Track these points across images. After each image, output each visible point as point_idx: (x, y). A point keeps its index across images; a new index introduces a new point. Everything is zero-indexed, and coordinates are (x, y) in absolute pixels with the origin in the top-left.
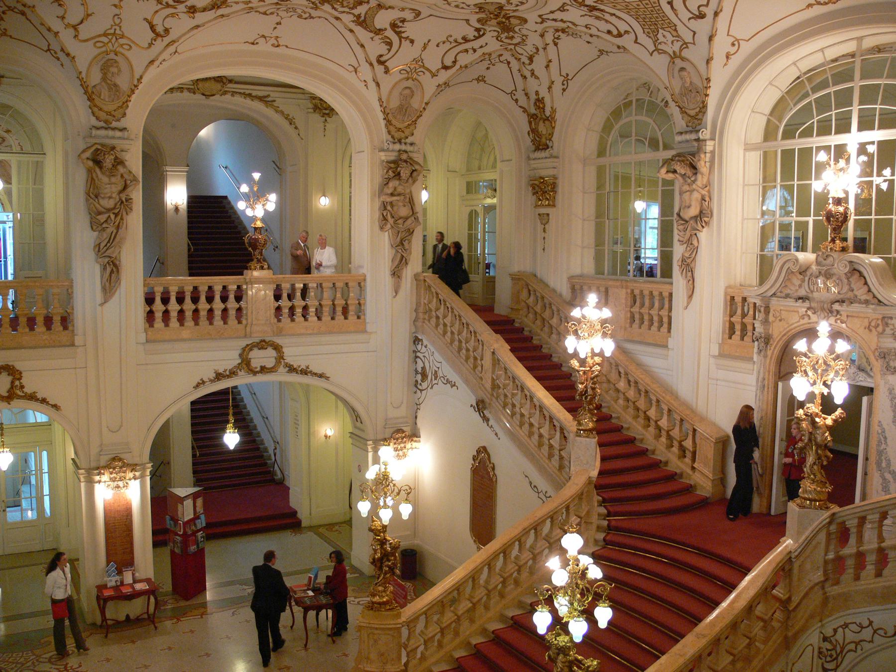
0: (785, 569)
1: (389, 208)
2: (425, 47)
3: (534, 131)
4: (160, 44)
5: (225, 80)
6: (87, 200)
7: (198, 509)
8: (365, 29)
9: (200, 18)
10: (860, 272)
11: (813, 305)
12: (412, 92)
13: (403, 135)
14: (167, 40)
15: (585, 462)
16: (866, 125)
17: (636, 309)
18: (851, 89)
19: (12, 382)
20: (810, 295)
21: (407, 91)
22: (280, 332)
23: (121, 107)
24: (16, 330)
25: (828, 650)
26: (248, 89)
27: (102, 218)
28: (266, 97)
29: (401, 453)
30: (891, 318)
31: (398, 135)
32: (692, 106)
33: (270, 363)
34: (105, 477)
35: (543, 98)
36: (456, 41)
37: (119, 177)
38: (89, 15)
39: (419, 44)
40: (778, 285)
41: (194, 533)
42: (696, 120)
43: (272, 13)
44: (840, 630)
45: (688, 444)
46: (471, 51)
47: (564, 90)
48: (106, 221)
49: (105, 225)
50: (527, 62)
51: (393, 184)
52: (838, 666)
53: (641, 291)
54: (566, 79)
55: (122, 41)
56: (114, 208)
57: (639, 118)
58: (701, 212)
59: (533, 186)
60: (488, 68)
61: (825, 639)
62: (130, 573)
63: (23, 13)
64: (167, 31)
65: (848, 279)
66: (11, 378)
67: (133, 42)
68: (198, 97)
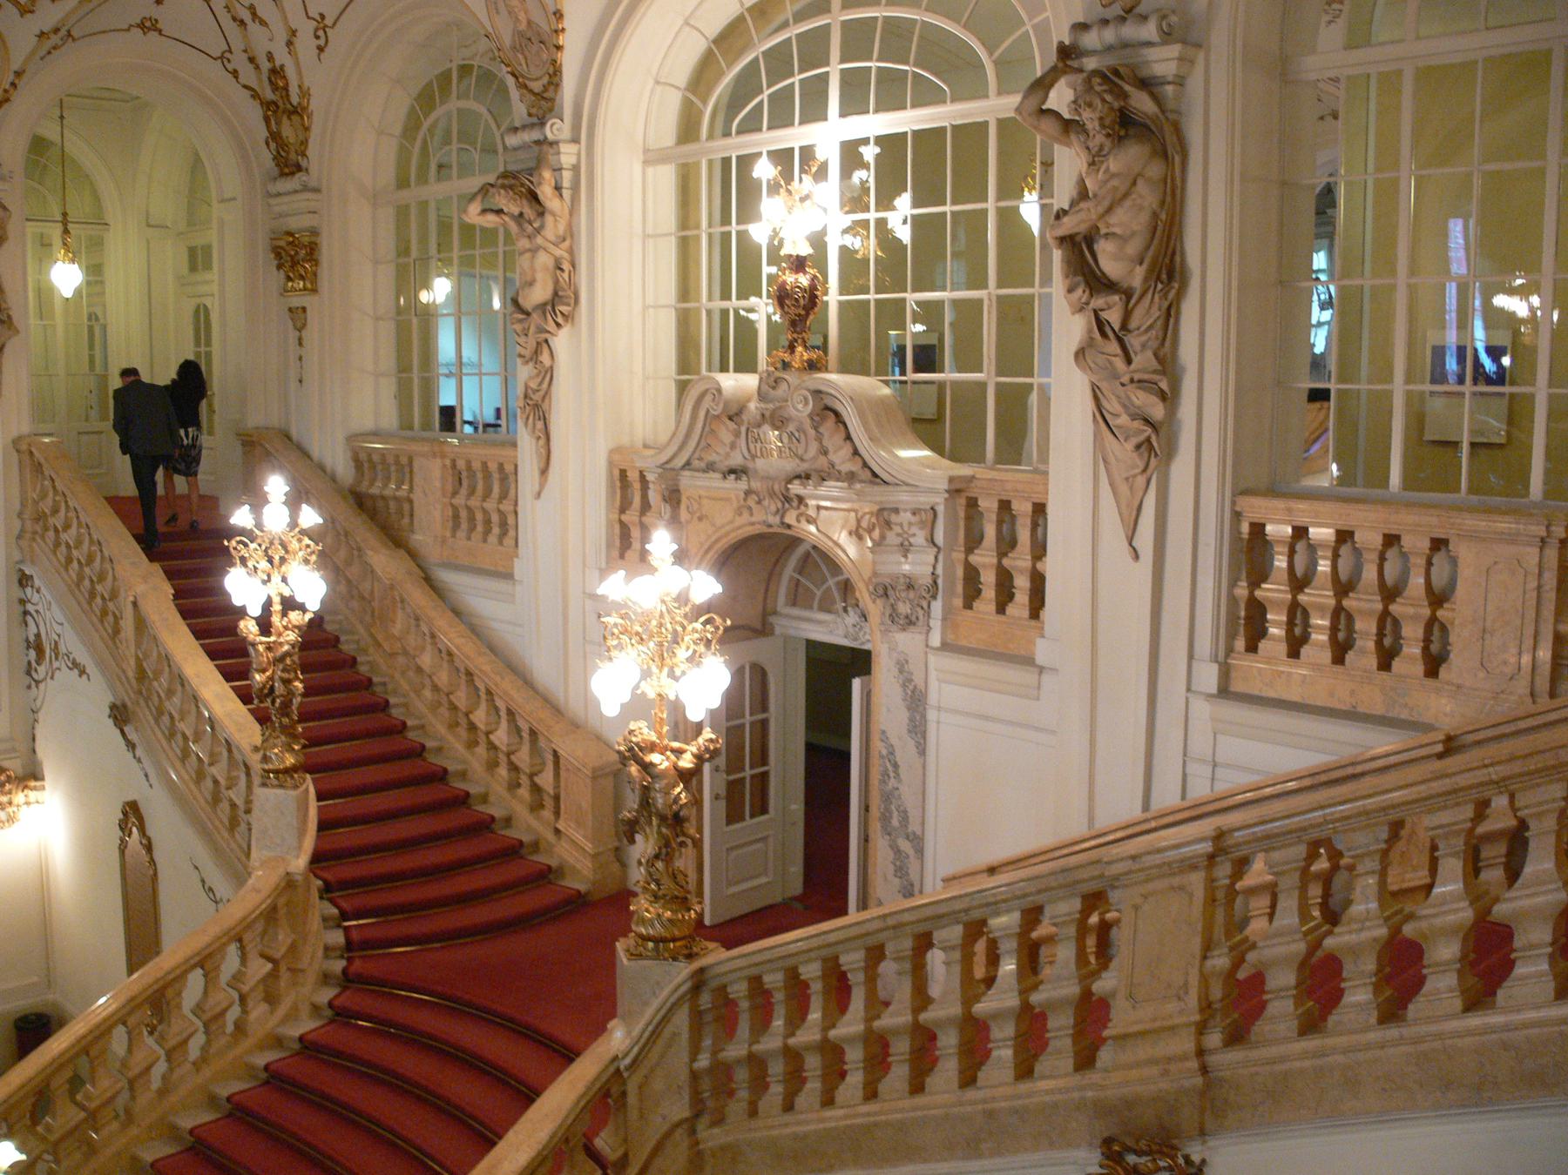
0: (606, 1100)
10: (837, 414)
11: (755, 485)
16: (853, 104)
17: (459, 500)
18: (826, 29)
20: (750, 465)
30: (896, 511)
32: (539, 73)
35: (282, 66)
40: (692, 444)
42: (544, 102)
45: (546, 780)
47: (321, 49)
53: (469, 463)
54: (322, 27)
57: (462, 104)
58: (556, 294)
59: (277, 252)
65: (816, 428)
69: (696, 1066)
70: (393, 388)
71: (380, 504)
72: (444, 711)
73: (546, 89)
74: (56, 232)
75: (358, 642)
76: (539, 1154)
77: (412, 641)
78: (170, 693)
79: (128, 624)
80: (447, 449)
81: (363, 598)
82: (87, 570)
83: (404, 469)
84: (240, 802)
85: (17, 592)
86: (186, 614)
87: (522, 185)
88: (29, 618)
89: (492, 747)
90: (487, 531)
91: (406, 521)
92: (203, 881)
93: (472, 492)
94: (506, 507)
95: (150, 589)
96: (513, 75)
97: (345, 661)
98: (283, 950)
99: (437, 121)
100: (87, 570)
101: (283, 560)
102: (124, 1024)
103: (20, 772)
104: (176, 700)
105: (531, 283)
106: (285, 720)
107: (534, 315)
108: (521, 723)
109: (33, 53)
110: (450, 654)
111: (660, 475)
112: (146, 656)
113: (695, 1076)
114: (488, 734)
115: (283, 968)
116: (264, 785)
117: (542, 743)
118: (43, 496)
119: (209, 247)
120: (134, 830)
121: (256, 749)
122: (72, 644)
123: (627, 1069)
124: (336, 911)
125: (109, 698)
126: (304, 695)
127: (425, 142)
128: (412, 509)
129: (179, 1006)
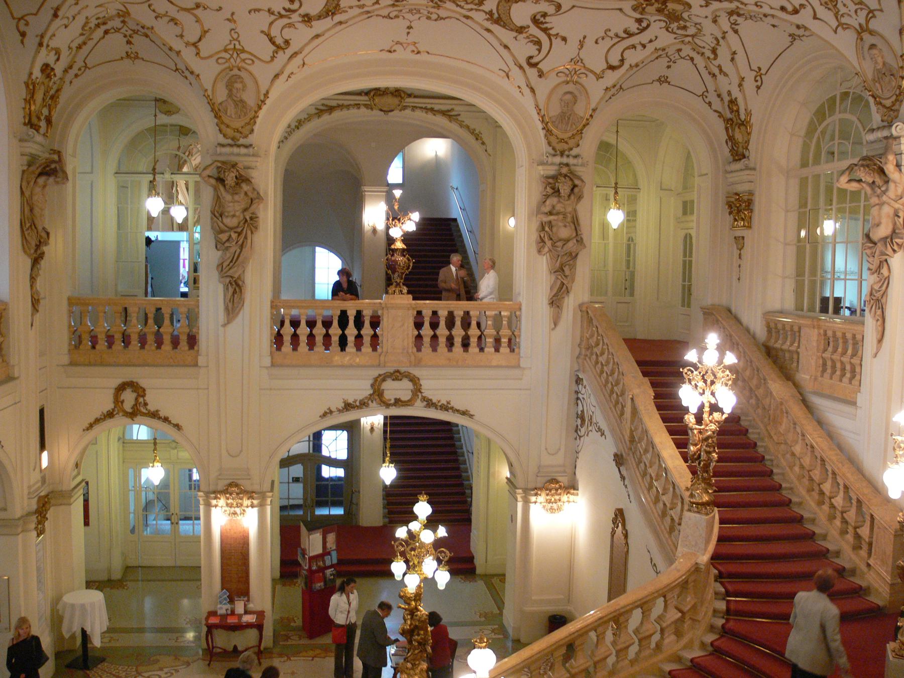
1: (547, 229)
2: (581, 44)
3: (731, 138)
4: (282, 57)
5: (403, 95)
6: (212, 219)
7: (328, 545)
8: (504, 27)
9: (319, 26)
12: (575, 97)
13: (566, 147)
14: (289, 52)
15: (693, 543)
17: (827, 355)
19: (136, 399)
21: (568, 97)
22: (418, 363)
23: (248, 124)
24: (328, 349)
26: (429, 103)
27: (224, 237)
28: (449, 111)
29: (555, 506)
31: (559, 147)
32: (888, 95)
33: (406, 396)
34: (222, 502)
35: (736, 99)
36: (617, 35)
37: (242, 195)
38: (206, 32)
39: (573, 43)
41: (322, 570)
43: (397, 17)
45: (864, 532)
46: (639, 47)
47: (758, 88)
48: (228, 240)
49: (227, 244)
50: (712, 56)
51: (553, 201)
53: (834, 332)
54: (759, 75)
55: (243, 56)
56: (237, 227)
57: (842, 116)
58: (894, 231)
59: (730, 205)
60: (669, 67)
62: (242, 603)
63: (147, 36)
64: (287, 42)
66: (135, 395)
67: (255, 56)
68: (376, 112)
70: (793, 286)
71: (780, 353)
72: (806, 481)
73: (893, 104)
74: (612, 192)
75: (759, 434)
77: (790, 436)
78: (646, 451)
79: (628, 410)
80: (822, 324)
81: (764, 408)
82: (610, 378)
83: (795, 333)
85: (575, 388)
86: (659, 407)
87: (875, 165)
88: (579, 402)
89: (832, 506)
90: (843, 375)
91: (795, 364)
92: (651, 559)
93: (835, 351)
94: (855, 361)
95: (642, 393)
96: (873, 96)
97: (750, 444)
98: (689, 607)
99: (828, 125)
100: (610, 378)
101: (713, 383)
102: (596, 631)
103: (566, 484)
104: (649, 456)
105: (878, 225)
106: (705, 475)
107: (879, 244)
108: (852, 494)
109: (602, 98)
110: (812, 447)
112: (636, 429)
114: (830, 498)
115: (687, 617)
116: (689, 510)
118: (592, 336)
119: (692, 202)
121: (687, 489)
122: (599, 418)
124: (723, 590)
125: (614, 450)
126: (717, 461)
127: (819, 138)
128: (798, 358)
129: (626, 627)
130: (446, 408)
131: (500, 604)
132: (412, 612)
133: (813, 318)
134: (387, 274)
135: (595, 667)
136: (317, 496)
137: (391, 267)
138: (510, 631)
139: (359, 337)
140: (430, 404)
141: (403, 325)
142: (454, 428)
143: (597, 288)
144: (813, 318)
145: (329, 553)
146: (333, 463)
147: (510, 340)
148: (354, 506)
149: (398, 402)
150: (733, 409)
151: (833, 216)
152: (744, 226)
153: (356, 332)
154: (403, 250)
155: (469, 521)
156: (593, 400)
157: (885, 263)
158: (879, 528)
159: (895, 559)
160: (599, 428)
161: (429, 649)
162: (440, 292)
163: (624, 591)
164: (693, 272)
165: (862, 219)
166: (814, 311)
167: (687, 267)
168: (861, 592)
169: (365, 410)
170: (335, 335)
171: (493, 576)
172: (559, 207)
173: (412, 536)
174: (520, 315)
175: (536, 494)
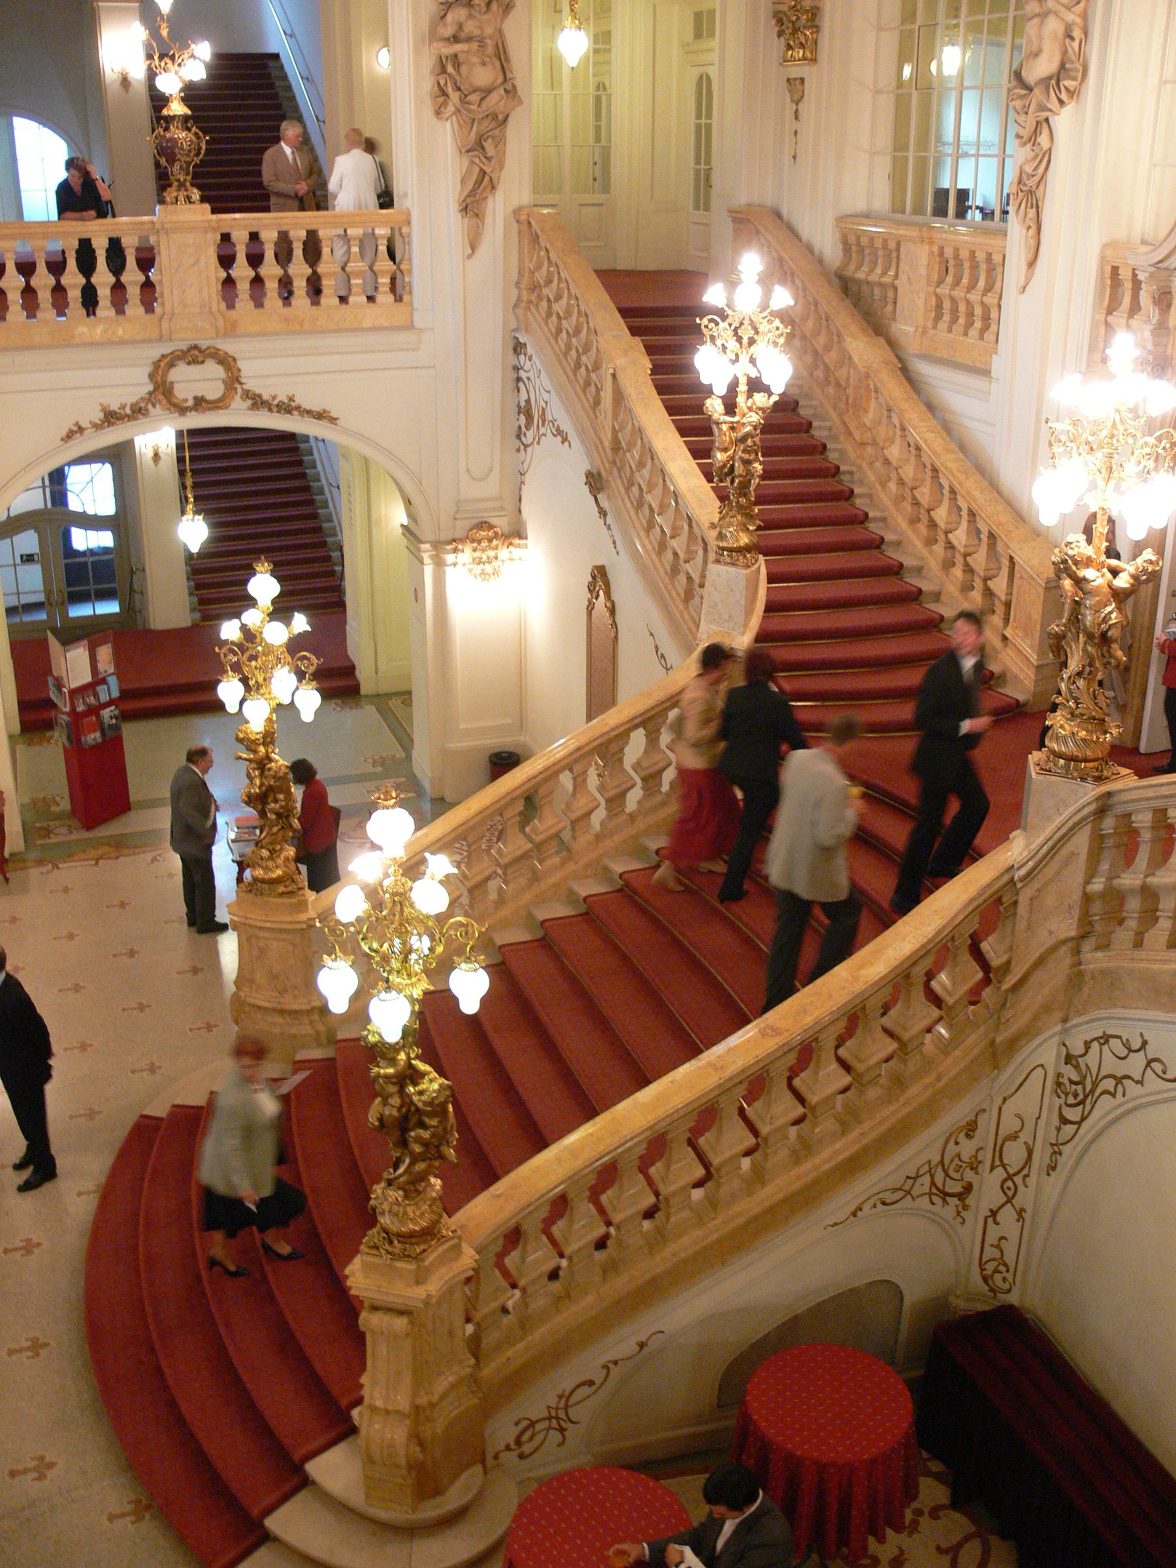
1: (450, 69)
7: (101, 667)
15: (725, 616)
17: (944, 290)
22: (231, 331)
24: (64, 315)
25: (1072, 1082)
29: (488, 568)
33: (214, 391)
44: (1095, 1045)
52: (1083, 1119)
53: (956, 250)
58: (1062, 66)
61: (1069, 1059)
69: (1090, 888)
71: (865, 288)
72: (907, 506)
75: (830, 429)
76: (923, 946)
77: (882, 433)
78: (641, 465)
79: (607, 395)
80: (936, 235)
81: (838, 385)
82: (584, 358)
83: (892, 253)
84: (696, 577)
85: (512, 359)
86: (661, 389)
88: (521, 384)
89: (950, 546)
90: (970, 324)
91: (889, 308)
92: (657, 647)
93: (957, 282)
94: (990, 299)
95: (630, 362)
97: (815, 447)
100: (574, 340)
101: (752, 342)
102: (571, 770)
103: (506, 529)
104: (646, 472)
105: (1036, 55)
106: (743, 500)
107: (1036, 91)
110: (918, 448)
111: (1152, 275)
112: (622, 428)
113: (1087, 898)
114: (947, 533)
116: (718, 561)
117: (1000, 548)
118: (539, 267)
119: (712, 13)
120: (601, 592)
121: (713, 526)
122: (557, 412)
123: (1022, 880)
126: (763, 477)
129: (621, 760)
130: (286, 408)
131: (406, 742)
132: (262, 764)
133: (921, 226)
134: (157, 165)
135: (573, 830)
136: (69, 585)
137: (166, 152)
138: (426, 784)
139: (118, 288)
140: (258, 402)
141: (197, 261)
142: (302, 446)
143: (543, 182)
144: (921, 226)
145: (103, 681)
146: (92, 522)
147: (393, 280)
148: (137, 596)
149: (200, 403)
150: (788, 386)
151: (960, 39)
152: (804, 58)
153: (112, 279)
154: (186, 118)
155: (341, 605)
156: (545, 381)
157: (1045, 125)
158: (1021, 578)
159: (1045, 623)
160: (558, 429)
161: (296, 823)
162: (266, 197)
163: (613, 703)
164: (714, 153)
165: (1009, 46)
166: (924, 213)
167: (703, 136)
168: (992, 682)
169: (142, 421)
170: (74, 286)
171: (389, 696)
172: (470, 27)
173: (249, 635)
174: (409, 234)
175: (455, 550)
